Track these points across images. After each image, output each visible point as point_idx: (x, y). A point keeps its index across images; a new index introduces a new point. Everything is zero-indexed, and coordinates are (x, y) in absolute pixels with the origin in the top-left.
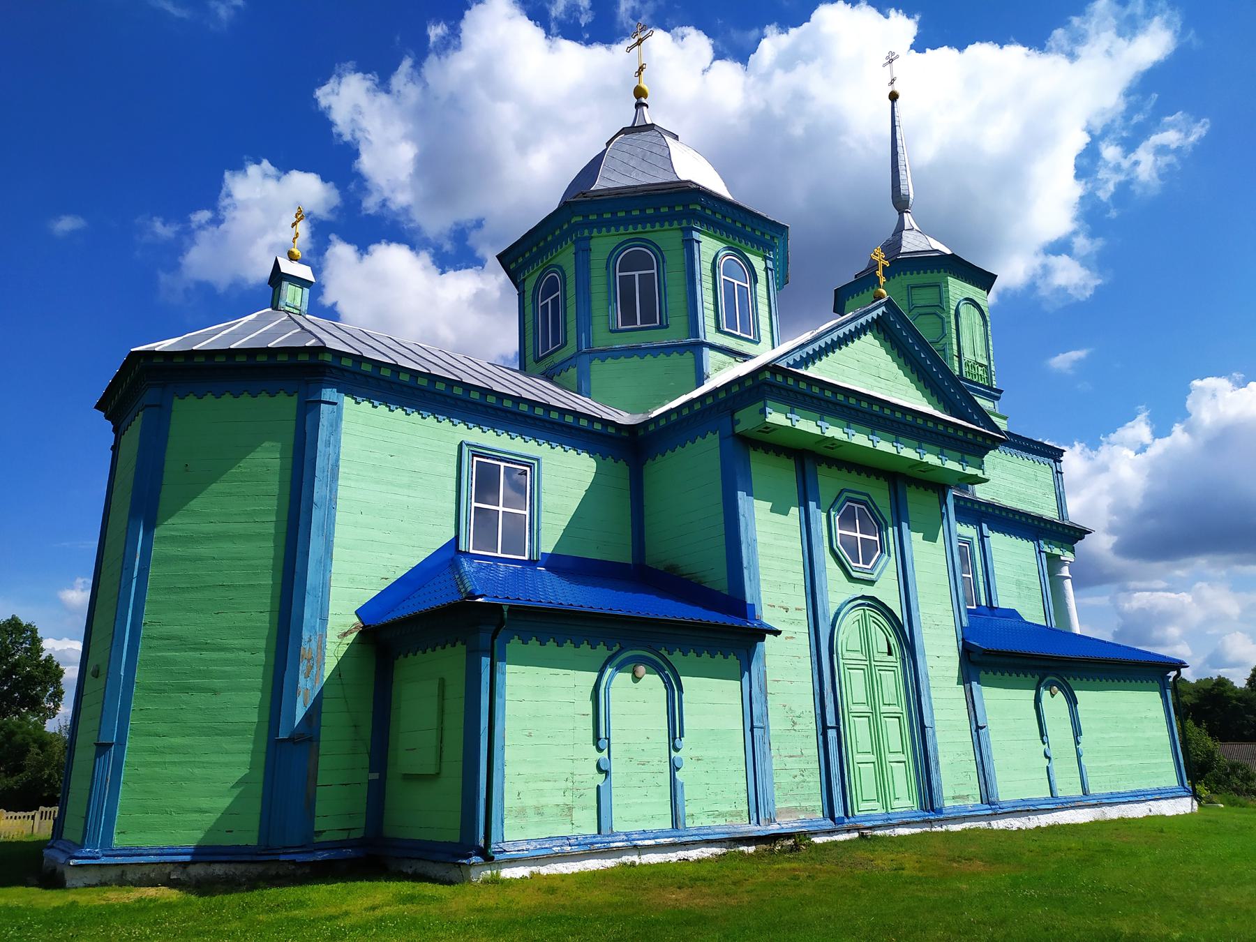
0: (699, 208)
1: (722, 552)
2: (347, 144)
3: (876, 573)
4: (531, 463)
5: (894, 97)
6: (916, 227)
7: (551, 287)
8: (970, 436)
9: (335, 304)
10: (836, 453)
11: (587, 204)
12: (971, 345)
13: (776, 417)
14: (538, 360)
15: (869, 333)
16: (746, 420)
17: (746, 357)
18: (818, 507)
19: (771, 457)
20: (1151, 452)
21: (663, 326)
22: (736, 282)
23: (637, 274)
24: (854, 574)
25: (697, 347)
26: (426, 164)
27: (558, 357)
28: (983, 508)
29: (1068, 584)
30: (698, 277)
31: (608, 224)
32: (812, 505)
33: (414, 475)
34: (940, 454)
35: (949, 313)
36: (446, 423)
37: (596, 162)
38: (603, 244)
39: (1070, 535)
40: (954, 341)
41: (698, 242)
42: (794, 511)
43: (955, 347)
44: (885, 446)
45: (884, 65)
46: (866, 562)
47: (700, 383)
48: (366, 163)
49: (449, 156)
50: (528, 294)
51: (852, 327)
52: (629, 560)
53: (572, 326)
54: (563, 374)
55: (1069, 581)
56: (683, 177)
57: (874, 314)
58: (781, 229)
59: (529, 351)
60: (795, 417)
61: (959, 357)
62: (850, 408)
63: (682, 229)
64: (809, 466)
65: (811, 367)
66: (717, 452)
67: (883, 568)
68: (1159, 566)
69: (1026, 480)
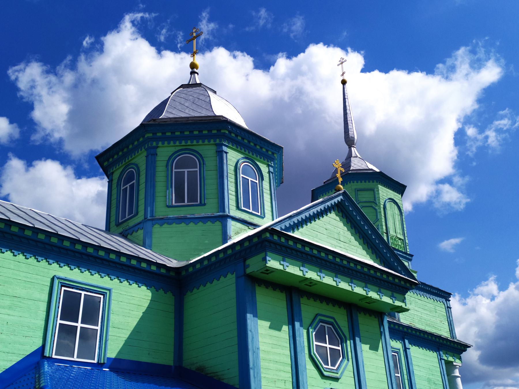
0: (227, 132)
1: (235, 357)
2: (27, 103)
3: (340, 372)
4: (105, 292)
5: (344, 82)
6: (359, 156)
7: (130, 177)
8: (397, 280)
9: (8, 195)
10: (313, 289)
11: (156, 128)
12: (393, 228)
13: (273, 264)
14: (118, 225)
15: (333, 212)
16: (253, 265)
17: (255, 226)
18: (301, 326)
19: (270, 292)
20: (498, 300)
21: (203, 204)
22: (250, 179)
23: (186, 171)
24: (326, 373)
25: (223, 218)
26: (74, 116)
27: (132, 223)
28: (405, 330)
29: (459, 380)
30: (225, 174)
31: (169, 139)
32: (297, 324)
33: (15, 299)
34: (378, 292)
35: (380, 207)
36: (44, 263)
37: (164, 104)
38: (164, 152)
39: (457, 348)
40: (384, 224)
41: (226, 153)
42: (285, 328)
43: (384, 227)
44: (344, 285)
45: (338, 65)
46: (333, 364)
47: (225, 241)
48: (37, 114)
49: (86, 109)
50: (115, 182)
51: (322, 207)
52: (171, 363)
53: (142, 202)
54: (134, 234)
55: (459, 379)
56: (217, 114)
57: (336, 200)
58: (278, 149)
59: (113, 218)
60: (286, 264)
61: (387, 233)
62: (321, 259)
63: (216, 145)
64: (295, 298)
65: (296, 232)
66: (234, 287)
67: (344, 369)
68: (507, 370)
69: (430, 311)
